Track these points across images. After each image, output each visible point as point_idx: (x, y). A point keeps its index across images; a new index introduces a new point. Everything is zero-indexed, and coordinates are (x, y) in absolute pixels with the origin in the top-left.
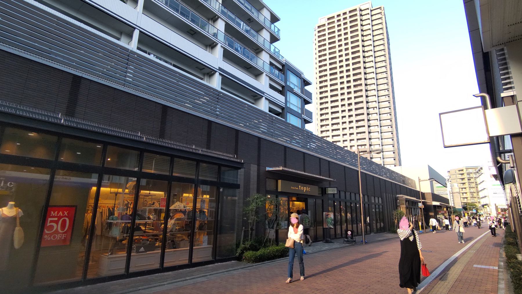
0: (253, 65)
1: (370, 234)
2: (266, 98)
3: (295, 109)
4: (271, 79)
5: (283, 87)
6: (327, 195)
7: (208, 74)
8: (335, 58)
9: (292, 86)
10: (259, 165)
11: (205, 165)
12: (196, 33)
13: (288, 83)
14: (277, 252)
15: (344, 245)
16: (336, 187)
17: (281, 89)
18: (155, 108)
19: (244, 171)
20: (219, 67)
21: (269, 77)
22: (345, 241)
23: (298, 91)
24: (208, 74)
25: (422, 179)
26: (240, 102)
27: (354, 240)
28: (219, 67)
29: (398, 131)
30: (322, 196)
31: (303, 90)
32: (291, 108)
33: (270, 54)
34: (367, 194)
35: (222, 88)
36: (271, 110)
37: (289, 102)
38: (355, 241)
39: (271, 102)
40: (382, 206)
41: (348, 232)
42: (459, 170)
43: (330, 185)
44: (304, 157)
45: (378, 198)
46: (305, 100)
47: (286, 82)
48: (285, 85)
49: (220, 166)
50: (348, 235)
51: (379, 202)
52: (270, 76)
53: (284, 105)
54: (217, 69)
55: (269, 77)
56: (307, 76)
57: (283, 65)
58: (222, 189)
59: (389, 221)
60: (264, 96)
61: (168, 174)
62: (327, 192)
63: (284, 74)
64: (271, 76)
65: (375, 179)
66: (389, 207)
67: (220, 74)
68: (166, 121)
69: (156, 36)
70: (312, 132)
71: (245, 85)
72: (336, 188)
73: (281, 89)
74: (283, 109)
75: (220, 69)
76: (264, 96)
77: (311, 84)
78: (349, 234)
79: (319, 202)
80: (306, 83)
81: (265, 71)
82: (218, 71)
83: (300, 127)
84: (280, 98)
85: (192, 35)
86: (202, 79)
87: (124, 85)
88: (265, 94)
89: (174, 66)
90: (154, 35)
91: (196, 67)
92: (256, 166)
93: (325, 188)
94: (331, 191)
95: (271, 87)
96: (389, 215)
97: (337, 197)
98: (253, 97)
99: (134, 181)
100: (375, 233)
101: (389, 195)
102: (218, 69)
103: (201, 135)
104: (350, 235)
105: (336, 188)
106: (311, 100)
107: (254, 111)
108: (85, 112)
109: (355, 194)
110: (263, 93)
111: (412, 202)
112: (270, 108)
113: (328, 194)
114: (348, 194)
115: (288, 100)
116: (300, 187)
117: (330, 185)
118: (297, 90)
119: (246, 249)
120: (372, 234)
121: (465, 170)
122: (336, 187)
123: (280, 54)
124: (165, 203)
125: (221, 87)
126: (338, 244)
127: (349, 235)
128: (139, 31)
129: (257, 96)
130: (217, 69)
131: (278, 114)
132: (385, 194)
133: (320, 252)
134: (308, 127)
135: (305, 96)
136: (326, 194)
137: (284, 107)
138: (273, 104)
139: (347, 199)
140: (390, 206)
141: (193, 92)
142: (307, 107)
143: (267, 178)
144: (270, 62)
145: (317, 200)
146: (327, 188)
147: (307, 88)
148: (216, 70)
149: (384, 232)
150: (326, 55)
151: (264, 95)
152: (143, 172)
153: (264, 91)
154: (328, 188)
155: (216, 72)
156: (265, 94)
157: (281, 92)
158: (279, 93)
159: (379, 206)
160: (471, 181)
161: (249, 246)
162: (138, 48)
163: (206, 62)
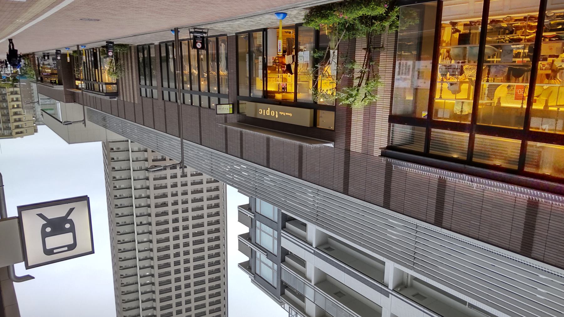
0: (301, 277)
1: (160, 43)
2: (312, 245)
3: (264, 227)
4: (303, 275)
5: (283, 261)
6: (230, 103)
7: (406, 287)
8: (196, 300)
9: (270, 263)
10: (347, 151)
11: (455, 156)
12: (335, 294)
13: (276, 266)
14: (327, 14)
15: (208, 27)
16: (217, 114)
17: (286, 258)
18: (546, 253)
19: (375, 141)
20: (388, 297)
21: (306, 278)
22: (205, 33)
23: (260, 255)
24: (406, 287)
25: (81, 124)
26: (375, 251)
27: (192, 35)
28: (388, 297)
29: (107, 190)
30: (238, 102)
31: (252, 255)
32: (272, 230)
33: (305, 313)
34: (164, 102)
35: (384, 263)
36: (303, 226)
37: (273, 237)
38: (191, 32)
39: (304, 239)
40: (140, 84)
41: (201, 46)
42: (22, 133)
43: (226, 118)
44: (135, 121)
45: (146, 96)
46: (250, 240)
47: (280, 270)
48: (281, 264)
49: (426, 154)
50: (201, 41)
51: (102, 86)
52: (305, 280)
53: (282, 234)
54: (392, 294)
55: (306, 278)
56: (245, 277)
57: (284, 295)
58: (423, 116)
59: (130, 64)
60: (314, 249)
61: (530, 143)
62: (232, 107)
63: (282, 282)
64: (303, 279)
65: (152, 123)
66: (129, 83)
67: (387, 286)
68: (524, 230)
69: (415, 307)
70: (239, 191)
71: (345, 268)
72: (218, 113)
73: (286, 258)
74: (284, 227)
75: (387, 294)
76: (314, 249)
77: (240, 264)
78: (199, 43)
79: (244, 92)
80: (247, 267)
81: (313, 288)
82: (391, 292)
83: (228, 186)
84: (288, 244)
85: (340, 292)
86: (416, 279)
87: (417, 226)
88: (313, 252)
89: (464, 303)
90: (415, 307)
91: (426, 298)
92: (352, 149)
93: (233, 113)
94: (226, 109)
95: (302, 262)
96: (130, 71)
97: (214, 100)
98: (331, 247)
99: (532, 128)
100: (153, 44)
101: (129, 101)
102: (390, 294)
103: (454, 203)
104: (197, 42)
105: (218, 113)
106: (240, 240)
107: (306, 215)
108: (483, 202)
109: (170, 100)
110: (315, 254)
111: (94, 89)
112: (305, 230)
113: (229, 104)
114: (196, 102)
115: (276, 242)
116: (277, 116)
117: (226, 118)
118: (261, 255)
119: (381, 18)
120: (157, 43)
121: (14, 133)
122: (217, 114)
123: (288, 313)
124: (519, 93)
125: (385, 265)
126: (217, 29)
127: (200, 42)
128: (389, 288)
129: (326, 249)
130: (392, 294)
131: (291, 220)
132: (136, 102)
133: (251, 16)
134: (245, 200)
135: (249, 246)
136: (233, 104)
137: (282, 231)
138: (299, 235)
139: (144, 89)
140: (127, 84)
141: (460, 272)
142: (245, 230)
143: (334, 131)
144: (304, 301)
145: (248, 96)
146: (231, 112)
147: (246, 259)
148: (393, 293)
149: (138, 46)
150: (209, 303)
151: (315, 251)
152: (520, 139)
153: (314, 256)
154: (230, 114)
155: (393, 290)
156: (313, 252)
157: (285, 253)
158: (290, 252)
159: (169, 87)
160: (6, 118)
161: (374, 24)
162: (384, 263)
163: (406, 303)
